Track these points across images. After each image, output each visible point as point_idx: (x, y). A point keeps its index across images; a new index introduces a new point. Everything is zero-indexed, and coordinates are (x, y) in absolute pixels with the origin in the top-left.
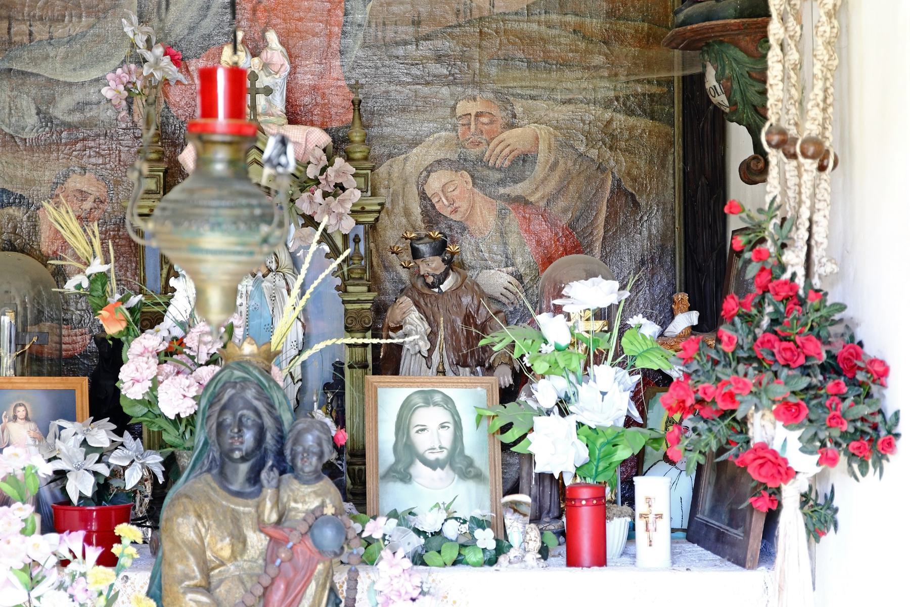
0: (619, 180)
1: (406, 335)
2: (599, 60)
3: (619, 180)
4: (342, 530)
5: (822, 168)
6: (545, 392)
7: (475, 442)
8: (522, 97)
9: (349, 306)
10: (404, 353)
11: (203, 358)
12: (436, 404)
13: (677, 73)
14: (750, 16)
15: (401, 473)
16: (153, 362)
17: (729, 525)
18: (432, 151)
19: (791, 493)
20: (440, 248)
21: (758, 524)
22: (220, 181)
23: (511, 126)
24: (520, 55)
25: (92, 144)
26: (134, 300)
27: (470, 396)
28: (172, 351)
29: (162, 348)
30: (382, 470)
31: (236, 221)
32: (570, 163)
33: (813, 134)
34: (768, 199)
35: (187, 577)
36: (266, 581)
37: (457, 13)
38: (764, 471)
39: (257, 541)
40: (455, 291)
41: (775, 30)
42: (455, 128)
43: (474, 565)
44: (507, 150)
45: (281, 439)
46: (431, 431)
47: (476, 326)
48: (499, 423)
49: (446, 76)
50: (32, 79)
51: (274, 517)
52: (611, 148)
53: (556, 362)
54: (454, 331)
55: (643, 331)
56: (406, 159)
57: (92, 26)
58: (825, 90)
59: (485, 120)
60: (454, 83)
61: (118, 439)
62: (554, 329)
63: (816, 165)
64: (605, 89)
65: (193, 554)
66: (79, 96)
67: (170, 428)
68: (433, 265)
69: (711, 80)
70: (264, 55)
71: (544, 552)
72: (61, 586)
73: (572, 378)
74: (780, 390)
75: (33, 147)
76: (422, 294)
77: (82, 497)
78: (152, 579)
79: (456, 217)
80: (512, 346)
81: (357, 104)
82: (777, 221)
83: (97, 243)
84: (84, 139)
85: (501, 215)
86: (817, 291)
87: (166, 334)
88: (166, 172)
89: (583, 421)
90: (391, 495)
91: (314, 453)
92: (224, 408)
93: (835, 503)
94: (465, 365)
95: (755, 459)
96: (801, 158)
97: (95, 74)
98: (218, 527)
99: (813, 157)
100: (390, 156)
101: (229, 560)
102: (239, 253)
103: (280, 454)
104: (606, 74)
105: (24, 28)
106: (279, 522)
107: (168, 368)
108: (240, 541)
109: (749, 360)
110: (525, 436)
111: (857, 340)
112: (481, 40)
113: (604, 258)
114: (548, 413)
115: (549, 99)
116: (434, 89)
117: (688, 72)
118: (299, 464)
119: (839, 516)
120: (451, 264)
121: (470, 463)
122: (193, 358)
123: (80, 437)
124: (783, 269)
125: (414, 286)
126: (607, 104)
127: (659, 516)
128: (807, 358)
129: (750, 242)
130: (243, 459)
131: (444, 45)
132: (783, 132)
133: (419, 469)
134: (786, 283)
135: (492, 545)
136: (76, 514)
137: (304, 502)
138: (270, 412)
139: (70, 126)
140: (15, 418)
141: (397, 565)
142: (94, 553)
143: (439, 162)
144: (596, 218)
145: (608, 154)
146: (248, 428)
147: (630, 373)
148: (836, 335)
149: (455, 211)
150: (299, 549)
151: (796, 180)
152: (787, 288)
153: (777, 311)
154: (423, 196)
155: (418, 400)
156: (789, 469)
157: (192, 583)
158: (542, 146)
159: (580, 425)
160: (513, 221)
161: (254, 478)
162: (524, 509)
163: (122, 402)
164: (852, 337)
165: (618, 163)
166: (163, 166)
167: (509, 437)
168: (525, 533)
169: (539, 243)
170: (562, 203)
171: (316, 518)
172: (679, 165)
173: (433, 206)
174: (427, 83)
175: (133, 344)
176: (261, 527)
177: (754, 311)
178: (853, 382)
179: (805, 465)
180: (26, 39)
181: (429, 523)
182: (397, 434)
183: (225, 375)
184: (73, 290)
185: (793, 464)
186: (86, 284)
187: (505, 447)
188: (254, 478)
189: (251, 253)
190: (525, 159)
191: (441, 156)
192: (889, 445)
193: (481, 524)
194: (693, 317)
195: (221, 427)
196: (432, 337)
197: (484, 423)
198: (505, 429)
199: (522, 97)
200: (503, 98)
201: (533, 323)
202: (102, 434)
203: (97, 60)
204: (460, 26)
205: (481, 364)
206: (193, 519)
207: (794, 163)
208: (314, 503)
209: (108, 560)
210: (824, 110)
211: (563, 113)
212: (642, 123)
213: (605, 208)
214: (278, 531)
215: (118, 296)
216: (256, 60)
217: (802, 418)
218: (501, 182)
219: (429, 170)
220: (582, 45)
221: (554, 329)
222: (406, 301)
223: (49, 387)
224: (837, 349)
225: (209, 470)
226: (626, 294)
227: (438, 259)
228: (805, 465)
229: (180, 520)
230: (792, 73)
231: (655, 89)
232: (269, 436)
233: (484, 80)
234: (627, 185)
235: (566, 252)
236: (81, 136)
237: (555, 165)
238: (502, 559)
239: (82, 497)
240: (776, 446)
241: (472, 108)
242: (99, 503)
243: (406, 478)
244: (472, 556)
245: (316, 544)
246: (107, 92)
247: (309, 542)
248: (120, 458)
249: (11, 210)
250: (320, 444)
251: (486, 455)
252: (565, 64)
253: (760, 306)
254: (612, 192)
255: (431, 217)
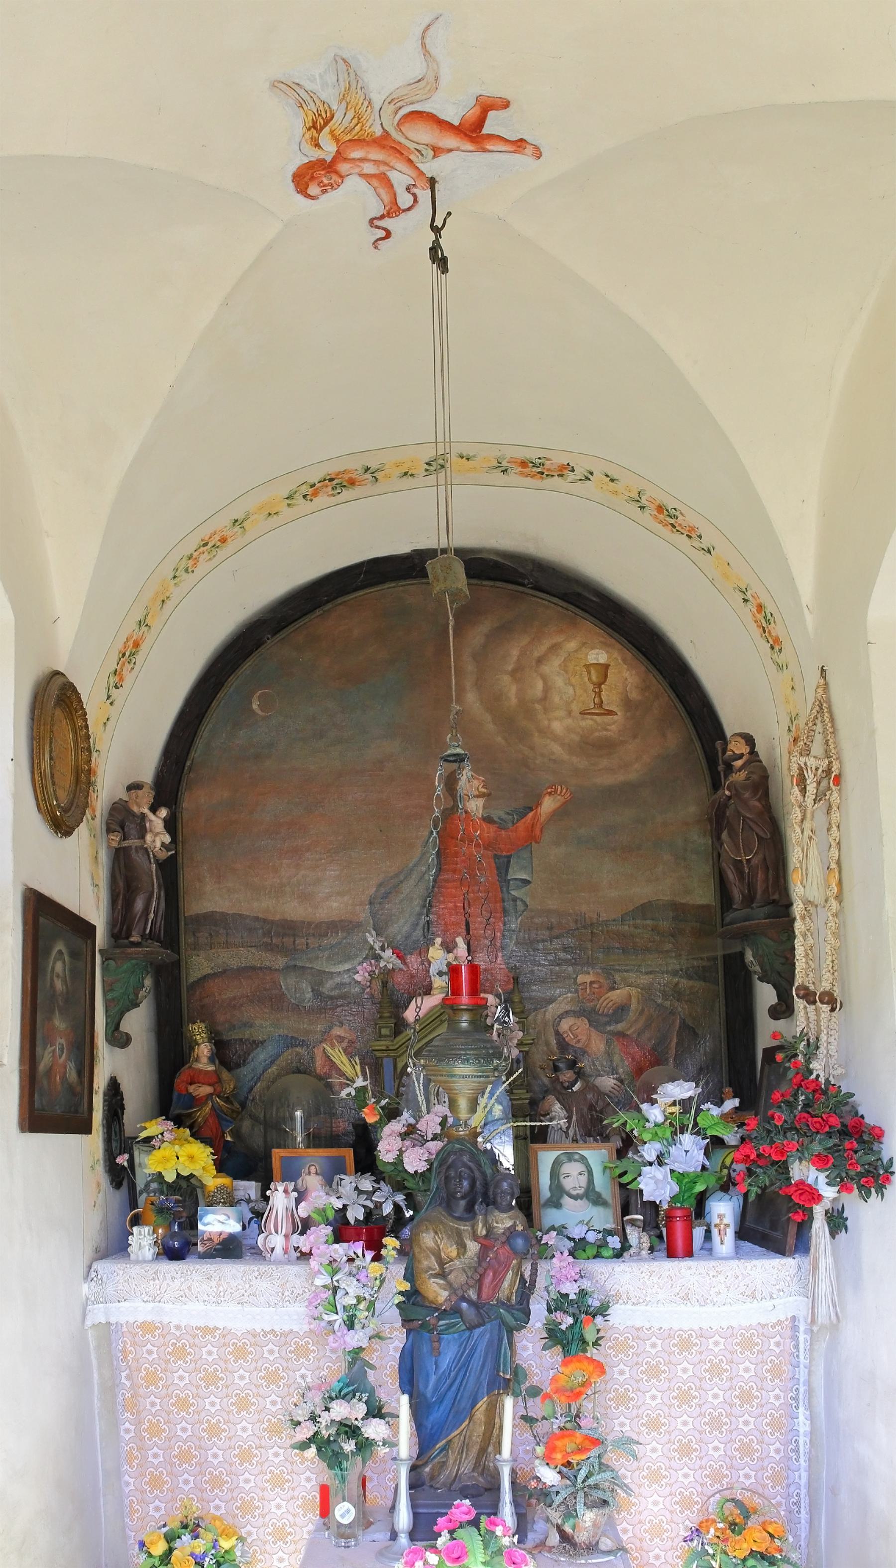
0: (684, 1020)
1: (551, 1120)
2: (668, 946)
3: (684, 1020)
4: (527, 1239)
5: (833, 1010)
6: (649, 1152)
7: (601, 1183)
8: (619, 971)
9: (515, 1102)
10: (549, 1130)
11: (430, 1136)
12: (576, 1161)
13: (720, 953)
14: (773, 918)
15: (555, 1203)
16: (399, 1139)
17: (771, 1229)
18: (563, 1005)
19: (819, 1211)
20: (572, 1064)
21: (792, 1230)
22: (465, 1033)
23: (613, 989)
24: (617, 945)
25: (346, 1008)
26: (383, 1102)
27: (597, 1156)
28: (410, 1132)
29: (403, 1131)
30: (542, 1201)
31: (477, 1057)
32: (652, 1010)
33: (827, 989)
34: (799, 1030)
35: (430, 1269)
36: (481, 1270)
37: (576, 922)
38: (803, 1198)
39: (473, 1247)
40: (581, 1091)
41: (799, 926)
42: (576, 991)
43: (607, 1258)
44: (611, 1003)
45: (486, 1185)
46: (573, 1177)
47: (596, 1111)
48: (618, 1172)
49: (570, 960)
50: (309, 971)
51: (484, 1232)
52: (678, 1000)
53: (656, 1133)
54: (582, 1116)
55: (711, 1112)
56: (545, 1012)
57: (345, 938)
58: (833, 961)
59: (595, 986)
60: (575, 964)
61: (376, 1186)
62: (655, 1114)
63: (829, 1008)
64: (674, 964)
65: (433, 1254)
66: (338, 980)
67: (410, 1179)
68: (567, 1076)
69: (749, 957)
70: (455, 951)
71: (652, 1249)
72: (350, 1274)
73: (665, 1143)
74: (817, 1148)
75: (310, 1011)
76: (561, 1093)
77: (356, 1220)
78: (406, 1269)
79: (579, 1045)
80: (625, 1124)
81: (516, 980)
82: (804, 1043)
83: (358, 1068)
84: (342, 1005)
85: (608, 1043)
86: (834, 1085)
87: (405, 1122)
88: (395, 1024)
89: (674, 1168)
90: (551, 1217)
91: (509, 1194)
92: (449, 1168)
93: (845, 1215)
94: (590, 1136)
95: (796, 1191)
96: (818, 1003)
97: (347, 966)
98: (448, 1238)
99: (827, 1003)
100: (535, 1009)
101: (455, 1258)
102: (480, 1077)
103: (485, 1195)
104: (674, 955)
105: (304, 940)
106: (486, 1236)
107: (407, 1143)
108: (462, 1247)
109: (791, 1129)
110: (636, 1178)
111: (860, 1115)
112: (592, 937)
113: (676, 1065)
114: (651, 1164)
115: (637, 971)
116: (564, 967)
117: (726, 953)
118: (499, 1200)
119: (848, 1223)
120: (580, 1074)
121: (599, 1195)
122: (423, 1136)
123: (354, 1185)
124: (811, 1072)
125: (555, 1089)
126: (675, 973)
127: (727, 1225)
128: (830, 1127)
129: (787, 1057)
130: (463, 1198)
131: (569, 941)
132: (806, 988)
133: (566, 1200)
134: (813, 1081)
135: (619, 1246)
136: (353, 1230)
137: (503, 1223)
138: (479, 1170)
139: (331, 998)
140: (309, 1173)
141: (564, 1260)
142: (369, 1255)
143: (567, 1012)
144: (670, 1043)
145: (676, 1004)
146: (465, 1179)
147: (703, 1139)
148: (846, 1112)
149: (579, 1041)
150: (501, 1251)
151: (815, 1018)
152: (814, 1084)
153: (807, 1098)
154: (557, 1033)
155: (563, 1158)
156: (820, 1195)
157: (433, 1272)
158: (634, 1000)
159: (672, 1171)
160: (617, 1047)
161: (470, 1209)
162: (639, 1223)
163: (378, 1163)
164: (857, 1113)
165: (682, 1009)
166: (393, 1021)
167: (625, 1179)
168: (640, 1238)
169: (633, 1059)
170: (647, 1035)
171: (511, 1233)
172: (723, 1009)
173: (564, 1039)
174: (558, 965)
175: (385, 1129)
176: (475, 1237)
177: (792, 1099)
178: (862, 1142)
179: (829, 1193)
180: (304, 947)
181: (577, 1232)
182: (551, 1179)
183: (449, 1147)
184: (344, 1097)
185: (824, 1194)
186: (353, 1094)
187: (623, 1186)
188: (470, 1209)
189: (487, 1077)
190: (621, 1010)
191: (568, 1008)
192: (887, 1180)
193: (610, 1233)
194: (736, 1102)
195: (447, 1178)
196: (569, 1118)
197: (608, 1171)
198: (622, 1175)
199: (619, 971)
200: (608, 972)
201: (639, 1110)
202: (367, 1184)
203: (348, 958)
204: (578, 929)
205: (601, 1135)
206: (432, 1234)
207: (814, 1007)
208: (509, 1224)
209: (377, 1258)
210: (833, 974)
211: (645, 980)
212: (698, 985)
213: (675, 1037)
214: (487, 1243)
215: (373, 1100)
216: (451, 955)
217: (830, 1164)
218: (609, 1023)
219: (561, 1017)
220: (657, 938)
221: (655, 1114)
222: (551, 1098)
223: (329, 1154)
224: (848, 1120)
225: (440, 1205)
226: (700, 1090)
227: (571, 1072)
228: (829, 1193)
229: (424, 1235)
230: (809, 952)
231: (705, 963)
232: (478, 1183)
233: (595, 962)
234: (689, 1022)
235: (652, 1065)
236: (339, 1003)
237: (643, 1010)
238: (625, 1254)
239: (356, 1220)
240: (810, 1181)
241: (588, 979)
242: (366, 1224)
243: (558, 1205)
244: (606, 1253)
245: (512, 1249)
246: (358, 977)
247: (507, 1247)
248: (379, 1197)
249: (298, 1049)
250: (512, 1188)
251: (609, 1192)
252: (647, 950)
253: (795, 1096)
254: (680, 1027)
255: (563, 1045)
